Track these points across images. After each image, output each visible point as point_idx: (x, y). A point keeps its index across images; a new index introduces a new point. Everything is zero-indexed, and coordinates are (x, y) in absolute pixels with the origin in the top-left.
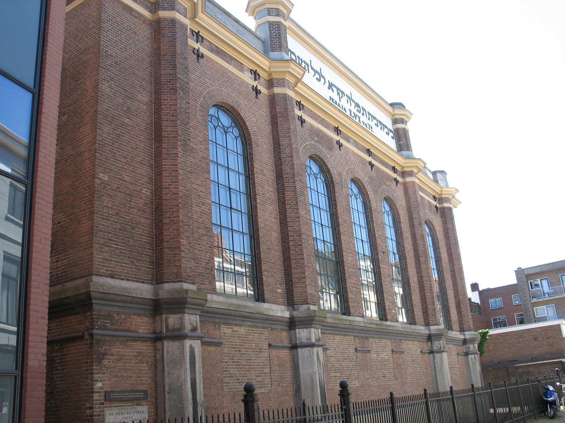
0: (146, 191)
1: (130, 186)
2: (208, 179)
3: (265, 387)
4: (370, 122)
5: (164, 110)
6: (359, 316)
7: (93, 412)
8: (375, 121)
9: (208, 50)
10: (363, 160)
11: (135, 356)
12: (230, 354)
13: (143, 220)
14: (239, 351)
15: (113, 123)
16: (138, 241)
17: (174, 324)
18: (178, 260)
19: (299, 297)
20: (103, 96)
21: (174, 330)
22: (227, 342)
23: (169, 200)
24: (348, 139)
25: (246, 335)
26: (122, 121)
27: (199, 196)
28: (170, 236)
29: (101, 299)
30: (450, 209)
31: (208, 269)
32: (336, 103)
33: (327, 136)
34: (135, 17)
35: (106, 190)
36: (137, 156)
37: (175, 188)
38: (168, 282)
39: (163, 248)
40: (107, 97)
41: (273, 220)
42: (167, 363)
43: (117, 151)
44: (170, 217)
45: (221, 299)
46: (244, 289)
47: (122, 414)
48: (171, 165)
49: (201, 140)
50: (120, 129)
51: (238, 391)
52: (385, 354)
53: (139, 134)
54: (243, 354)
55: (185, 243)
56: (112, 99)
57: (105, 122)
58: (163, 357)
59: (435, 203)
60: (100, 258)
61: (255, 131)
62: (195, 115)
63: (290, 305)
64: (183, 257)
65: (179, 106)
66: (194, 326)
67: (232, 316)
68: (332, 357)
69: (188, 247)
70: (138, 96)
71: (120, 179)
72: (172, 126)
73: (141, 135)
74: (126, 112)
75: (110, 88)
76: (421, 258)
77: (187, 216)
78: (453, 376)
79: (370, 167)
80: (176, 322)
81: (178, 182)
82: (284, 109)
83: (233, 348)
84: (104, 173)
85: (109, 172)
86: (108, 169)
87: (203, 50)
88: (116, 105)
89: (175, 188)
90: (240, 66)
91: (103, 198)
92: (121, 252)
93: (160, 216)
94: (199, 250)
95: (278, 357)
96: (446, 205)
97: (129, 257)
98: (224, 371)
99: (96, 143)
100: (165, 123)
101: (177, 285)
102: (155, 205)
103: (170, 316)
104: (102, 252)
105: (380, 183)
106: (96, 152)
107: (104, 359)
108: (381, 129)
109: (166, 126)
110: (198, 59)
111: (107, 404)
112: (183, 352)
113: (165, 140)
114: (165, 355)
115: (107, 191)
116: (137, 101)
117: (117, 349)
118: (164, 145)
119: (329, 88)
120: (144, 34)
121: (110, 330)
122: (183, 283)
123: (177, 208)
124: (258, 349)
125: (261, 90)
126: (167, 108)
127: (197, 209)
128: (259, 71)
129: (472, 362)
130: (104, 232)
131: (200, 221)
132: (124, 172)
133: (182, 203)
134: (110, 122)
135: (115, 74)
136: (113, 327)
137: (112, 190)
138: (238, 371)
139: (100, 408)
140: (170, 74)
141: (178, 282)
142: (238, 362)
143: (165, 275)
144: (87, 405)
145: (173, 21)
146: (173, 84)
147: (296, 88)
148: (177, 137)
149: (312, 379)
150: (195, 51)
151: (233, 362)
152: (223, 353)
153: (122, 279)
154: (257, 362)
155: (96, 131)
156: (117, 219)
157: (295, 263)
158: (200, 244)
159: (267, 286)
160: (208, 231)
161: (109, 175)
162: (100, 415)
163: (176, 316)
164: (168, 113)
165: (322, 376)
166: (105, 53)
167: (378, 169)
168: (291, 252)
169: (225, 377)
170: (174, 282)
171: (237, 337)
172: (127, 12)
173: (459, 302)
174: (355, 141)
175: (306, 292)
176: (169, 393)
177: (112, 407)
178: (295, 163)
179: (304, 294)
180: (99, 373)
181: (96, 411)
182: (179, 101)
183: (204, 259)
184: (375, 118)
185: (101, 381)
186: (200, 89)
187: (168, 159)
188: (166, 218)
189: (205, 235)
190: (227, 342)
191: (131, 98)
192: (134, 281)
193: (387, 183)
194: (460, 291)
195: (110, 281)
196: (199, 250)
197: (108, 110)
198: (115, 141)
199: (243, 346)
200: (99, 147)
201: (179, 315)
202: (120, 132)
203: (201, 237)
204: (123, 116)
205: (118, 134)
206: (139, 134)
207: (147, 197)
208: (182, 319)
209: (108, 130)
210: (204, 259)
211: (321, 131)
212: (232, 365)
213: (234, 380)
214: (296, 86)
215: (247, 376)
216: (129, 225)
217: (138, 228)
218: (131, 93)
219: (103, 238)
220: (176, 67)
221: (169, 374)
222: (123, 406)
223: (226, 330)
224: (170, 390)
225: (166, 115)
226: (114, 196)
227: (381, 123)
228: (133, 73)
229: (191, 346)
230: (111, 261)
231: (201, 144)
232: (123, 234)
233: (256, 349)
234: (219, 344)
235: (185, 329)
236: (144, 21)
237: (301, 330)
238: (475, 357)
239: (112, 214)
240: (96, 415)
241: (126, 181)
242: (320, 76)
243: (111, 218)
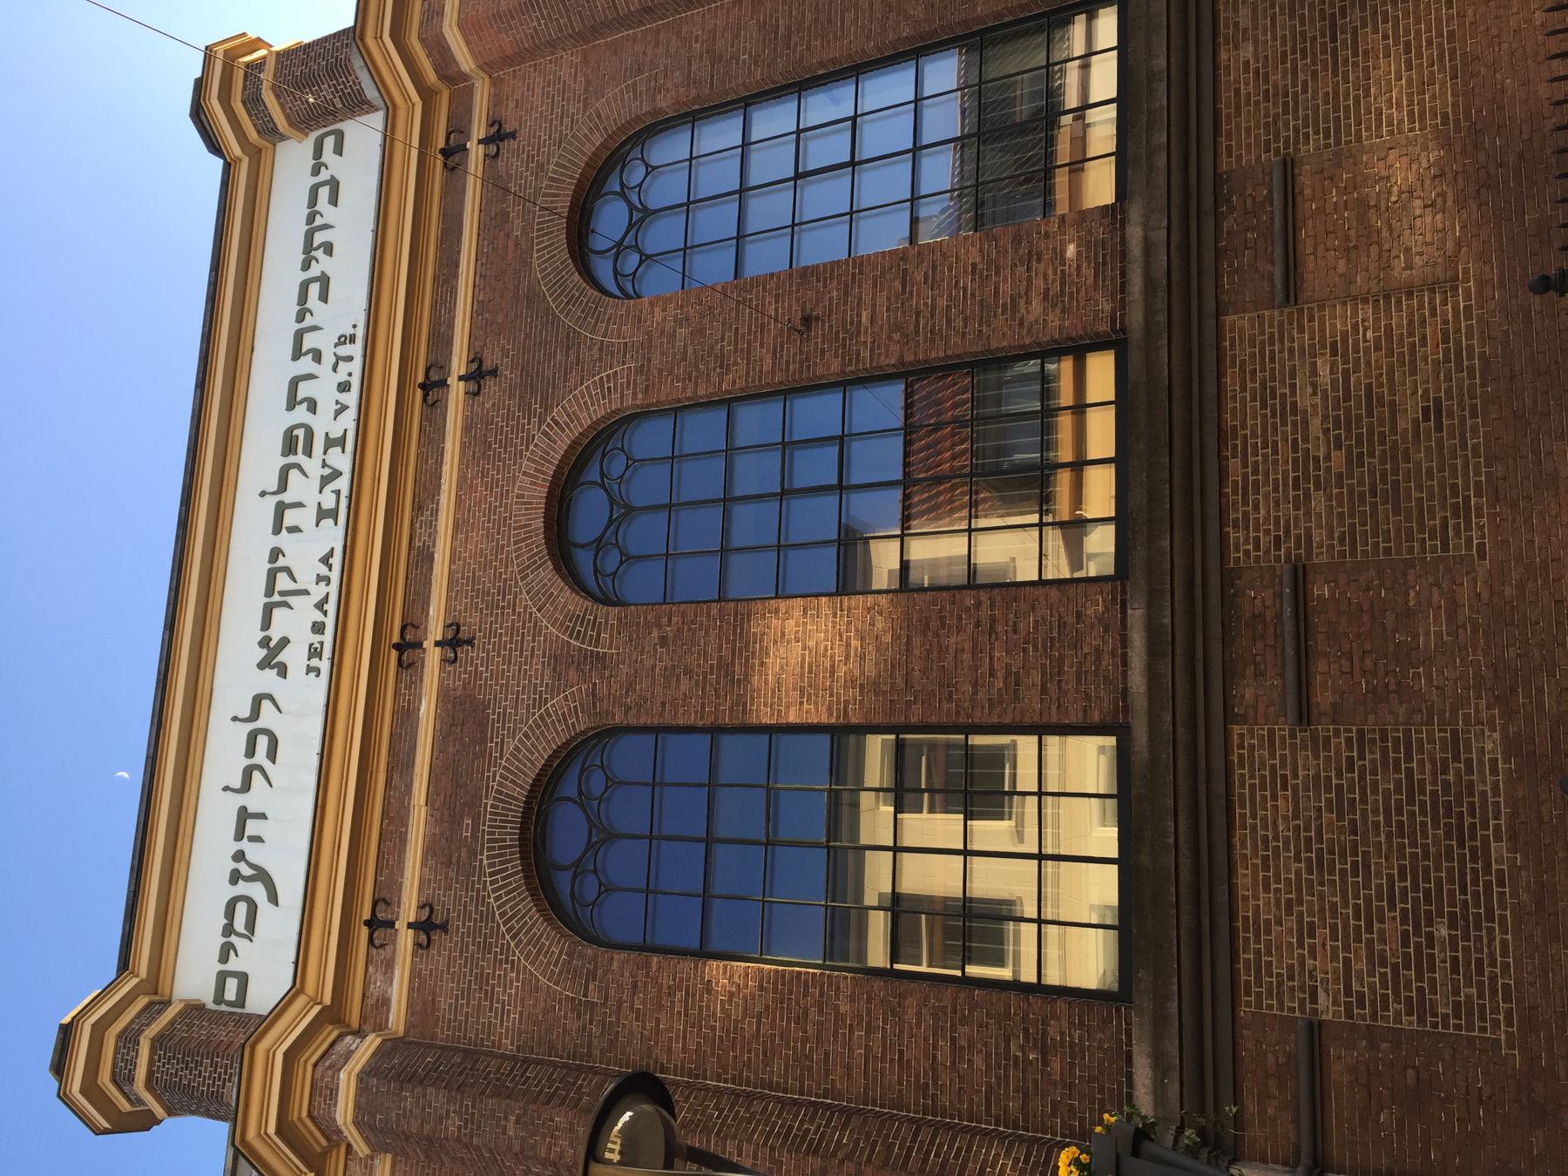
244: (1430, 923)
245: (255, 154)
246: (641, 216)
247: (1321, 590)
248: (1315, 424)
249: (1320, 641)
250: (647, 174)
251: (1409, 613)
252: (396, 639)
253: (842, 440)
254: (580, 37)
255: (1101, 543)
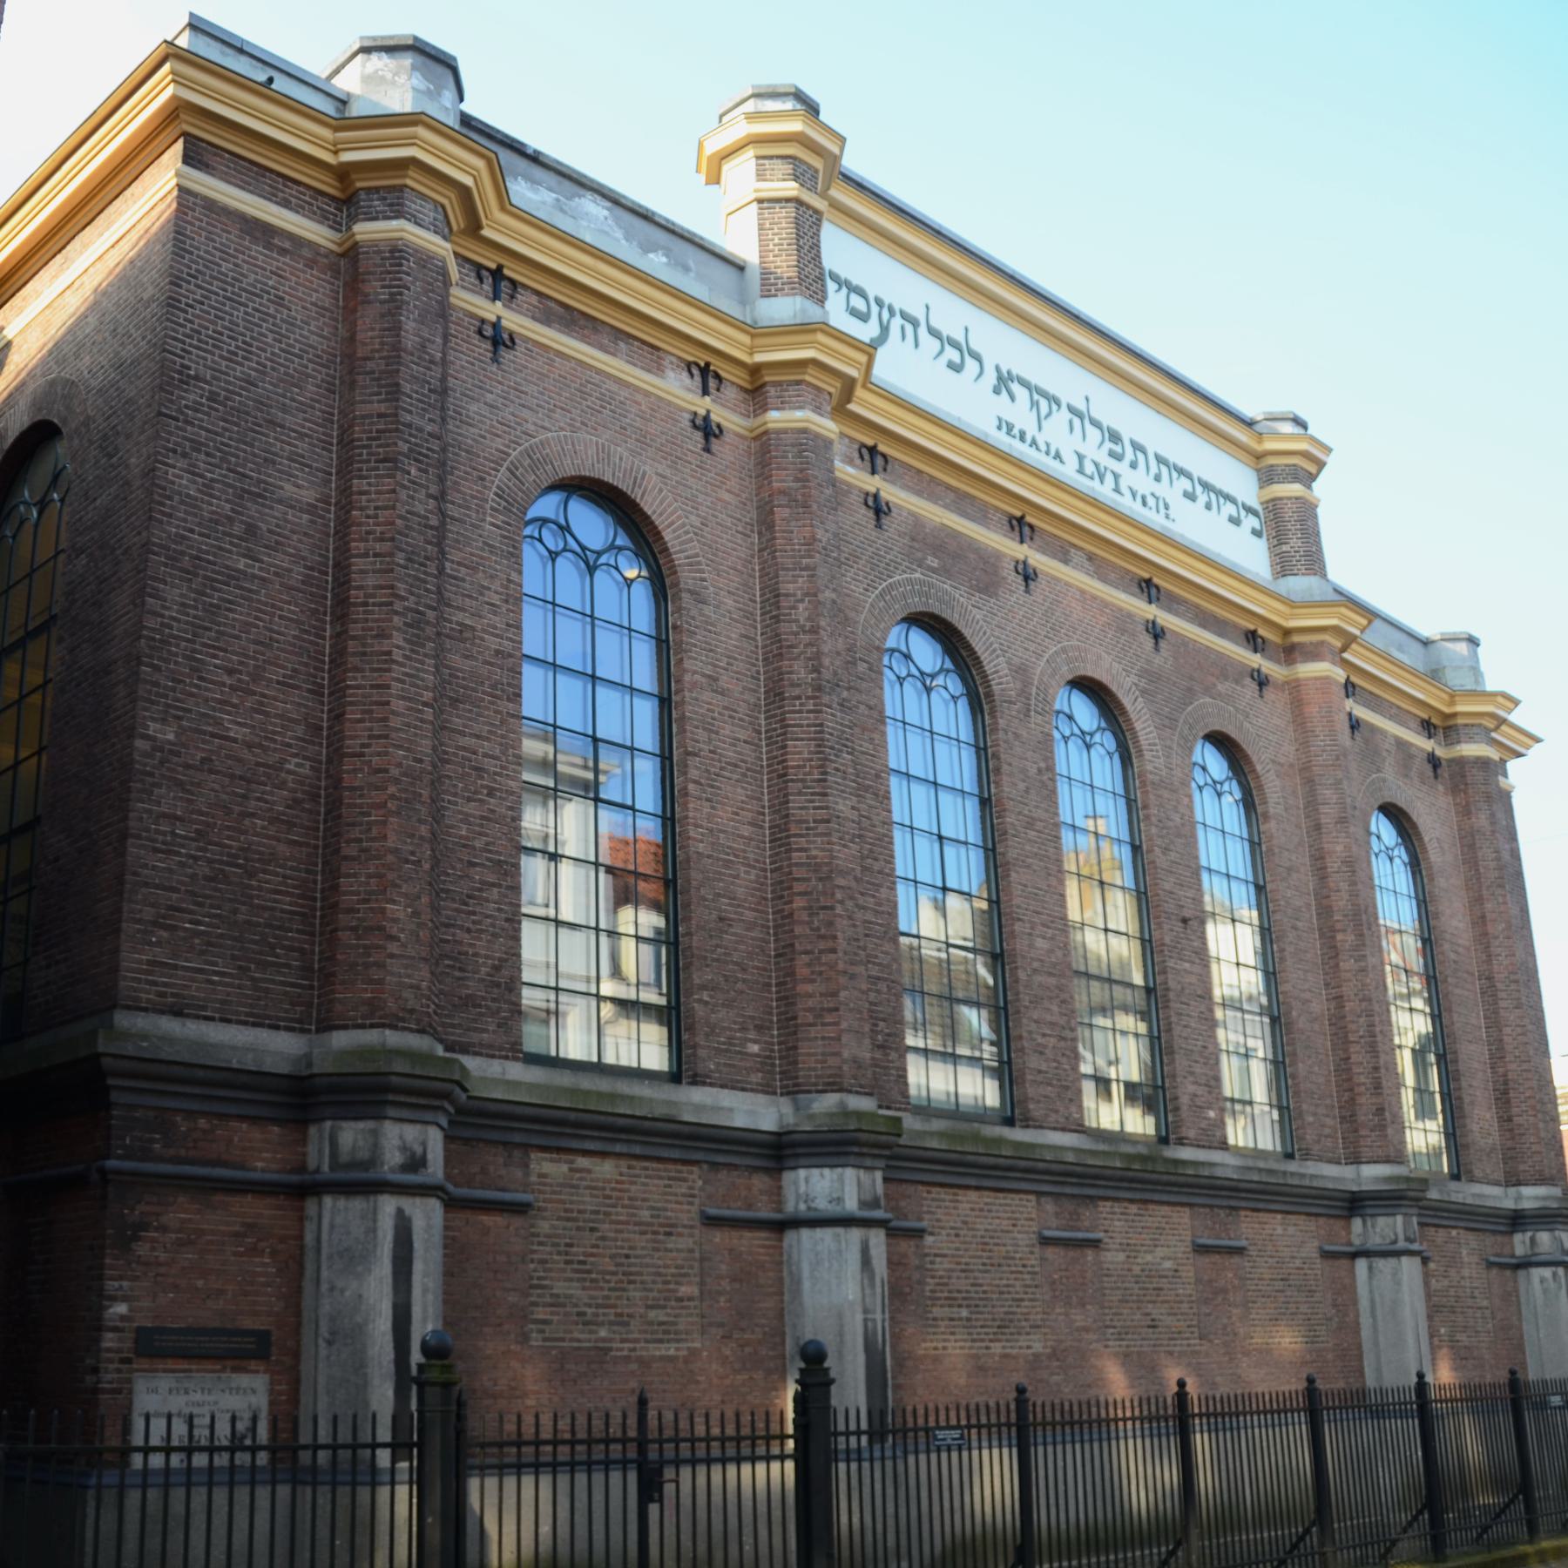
0: (297, 765)
1: (245, 754)
2: (513, 716)
3: (678, 1341)
4: (1162, 489)
5: (360, 524)
6: (1063, 1129)
7: (98, 1382)
8: (1185, 484)
9: (534, 318)
10: (1122, 620)
11: (237, 1235)
12: (557, 1236)
13: (283, 849)
14: (592, 1230)
15: (197, 575)
16: (264, 908)
17: (354, 1147)
18: (376, 964)
19: (815, 1069)
20: (170, 498)
21: (354, 1165)
22: (551, 1201)
23: (361, 788)
24: (1062, 553)
25: (617, 1182)
26: (227, 567)
27: (476, 769)
28: (358, 894)
29: (134, 1076)
30: (1492, 769)
31: (498, 985)
32: (1022, 437)
33: (972, 546)
34: (283, 251)
35: (169, 769)
36: (271, 663)
37: (379, 754)
38: (345, 1027)
39: (336, 930)
40: (182, 502)
41: (746, 831)
42: (330, 1257)
43: (207, 654)
44: (361, 840)
45: (535, 1075)
46: (647, 1048)
47: (186, 1392)
48: (372, 687)
49: (496, 599)
50: (220, 591)
51: (579, 1348)
52: (1160, 1252)
53: (282, 601)
54: (603, 1238)
55: (401, 916)
56: (195, 507)
57: (171, 575)
58: (318, 1240)
59: (1427, 745)
60: (140, 962)
61: (697, 555)
62: (478, 527)
63: (788, 1093)
64: (392, 956)
65: (401, 510)
66: (413, 1154)
67: (591, 1118)
68: (944, 1256)
69: (413, 927)
70: (282, 488)
71: (213, 735)
72: (379, 571)
73: (289, 603)
74: (240, 539)
75: (193, 474)
76: (1339, 937)
77: (412, 836)
78: (1459, 1337)
79: (1148, 642)
80: (361, 1143)
81: (386, 737)
82: (797, 480)
83: (568, 1220)
84: (164, 721)
85: (179, 718)
86: (178, 708)
87: (514, 321)
88: (211, 520)
89: (379, 754)
90: (652, 356)
91: (156, 791)
92: (209, 944)
93: (334, 835)
94: (469, 931)
95: (731, 1250)
96: (1471, 749)
97: (233, 957)
98: (532, 1287)
99: (140, 637)
100: (358, 563)
101: (370, 1037)
102: (326, 804)
103: (344, 1124)
104: (150, 943)
105: (1190, 690)
106: (140, 663)
107: (139, 1239)
108: (1208, 507)
109: (362, 572)
110: (495, 352)
111: (144, 1363)
112: (374, 1230)
113: (358, 613)
114: (325, 1236)
115: (173, 770)
116: (280, 502)
117: (181, 1212)
118: (355, 630)
119: (997, 391)
120: (311, 293)
121: (162, 1160)
122: (387, 1032)
123: (381, 812)
124: (661, 1225)
125: (724, 423)
126: (368, 517)
127: (471, 808)
128: (717, 365)
129: (1545, 1291)
130: (157, 887)
131: (478, 844)
132: (229, 714)
133: (399, 799)
134: (188, 572)
135: (208, 431)
136: (172, 1152)
137: (187, 766)
138: (584, 1288)
139: (119, 1371)
140: (380, 416)
141: (372, 1026)
142: (584, 1263)
143: (338, 1007)
144: (88, 1361)
145: (396, 252)
146: (388, 445)
147: (851, 407)
148: (391, 604)
149: (842, 1326)
150: (489, 331)
151: (567, 1262)
152: (533, 1235)
153: (206, 1018)
154: (653, 1266)
155: (143, 603)
156: (199, 849)
157: (809, 965)
158: (474, 913)
159: (707, 1035)
160: (506, 874)
161: (180, 727)
162: (119, 1391)
163: (361, 1125)
164: (368, 533)
165: (879, 1316)
166: (180, 373)
167: (1184, 642)
168: (798, 930)
169: (535, 1304)
170: (362, 1027)
171: (587, 1187)
172: (255, 240)
173: (1506, 1083)
174: (1091, 557)
175: (837, 1054)
176: (330, 1343)
177: (156, 1370)
178: (826, 649)
179: (832, 1061)
180: (121, 1278)
181: (109, 1377)
182: (403, 495)
183: (487, 957)
184: (1182, 472)
185: (125, 1299)
186: (498, 443)
187: (363, 671)
188: (348, 842)
189: (493, 885)
190: (551, 1201)
191: (260, 496)
192: (245, 1023)
193: (1219, 687)
194: (1509, 1048)
195: (169, 1025)
196: (469, 931)
197: (184, 537)
198: (200, 627)
199: (607, 1214)
200: (151, 648)
201: (370, 1124)
202: (220, 599)
203: (480, 890)
204: (230, 552)
205: (211, 605)
206: (282, 601)
207: (302, 783)
208: (375, 1133)
209: (182, 595)
210: (487, 957)
211: (956, 535)
212: (564, 1271)
213: (566, 1314)
214: (849, 401)
215: (614, 1306)
216: (238, 866)
217: (265, 872)
218: (260, 481)
219: (153, 905)
220: (398, 391)
221: (332, 1289)
222: (190, 1371)
223: (548, 1167)
224: (333, 1333)
225: (362, 540)
226: (192, 784)
227: (1206, 486)
228: (271, 422)
229: (400, 1213)
230: (175, 967)
231: (495, 613)
232: (216, 889)
233: (652, 1224)
234: (520, 1209)
235: (382, 1164)
236: (314, 262)
237: (815, 1172)
238: (1555, 1275)
239: (185, 837)
240: (104, 1391)
241: (235, 740)
242: (960, 355)
243: (183, 846)
244: (968, 1306)
245: (1259, 457)
246: (590, 564)
247: (1090, 1255)
248: (1149, 1258)
249: (1072, 1253)
250: (550, 552)
251: (1083, 1305)
252: (1029, 519)
253: (632, 808)
254: (1306, 768)
255: (575, 1043)
